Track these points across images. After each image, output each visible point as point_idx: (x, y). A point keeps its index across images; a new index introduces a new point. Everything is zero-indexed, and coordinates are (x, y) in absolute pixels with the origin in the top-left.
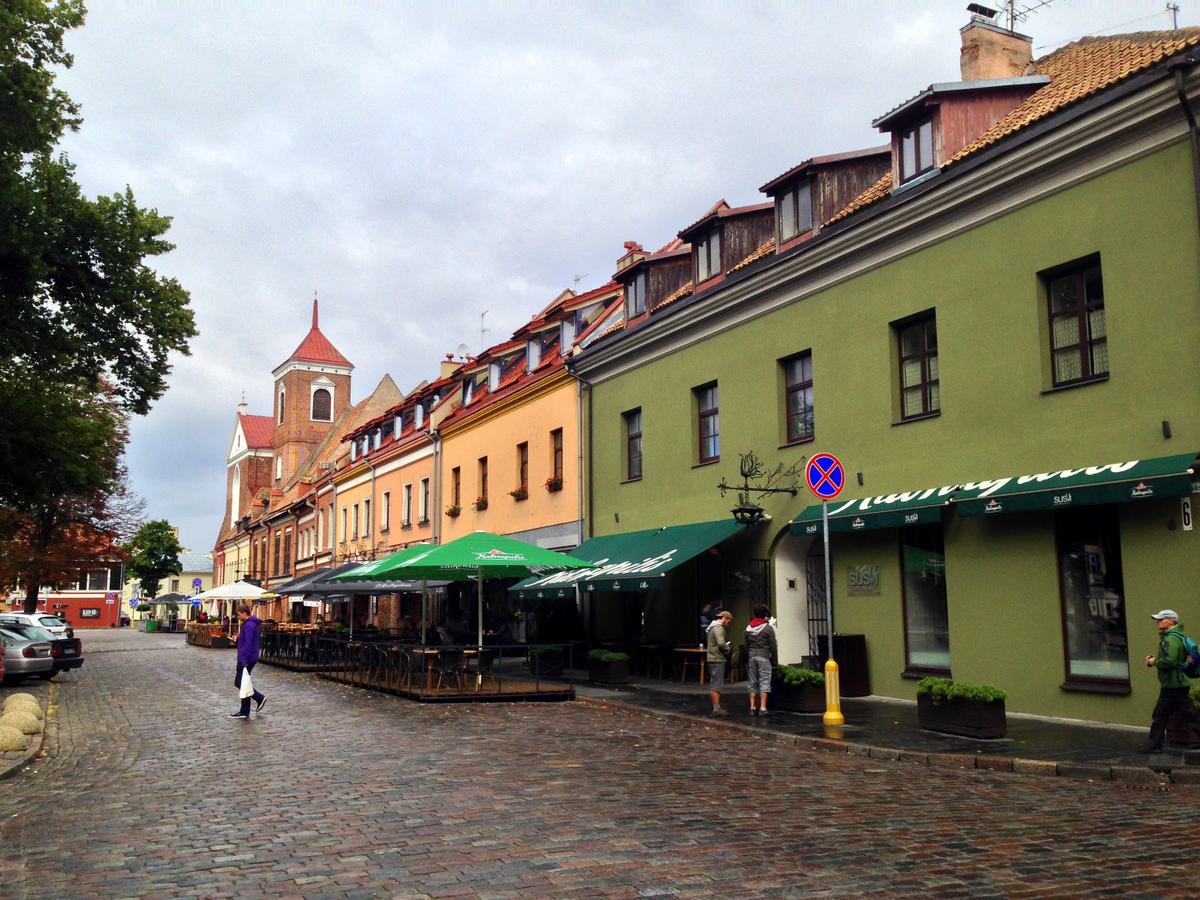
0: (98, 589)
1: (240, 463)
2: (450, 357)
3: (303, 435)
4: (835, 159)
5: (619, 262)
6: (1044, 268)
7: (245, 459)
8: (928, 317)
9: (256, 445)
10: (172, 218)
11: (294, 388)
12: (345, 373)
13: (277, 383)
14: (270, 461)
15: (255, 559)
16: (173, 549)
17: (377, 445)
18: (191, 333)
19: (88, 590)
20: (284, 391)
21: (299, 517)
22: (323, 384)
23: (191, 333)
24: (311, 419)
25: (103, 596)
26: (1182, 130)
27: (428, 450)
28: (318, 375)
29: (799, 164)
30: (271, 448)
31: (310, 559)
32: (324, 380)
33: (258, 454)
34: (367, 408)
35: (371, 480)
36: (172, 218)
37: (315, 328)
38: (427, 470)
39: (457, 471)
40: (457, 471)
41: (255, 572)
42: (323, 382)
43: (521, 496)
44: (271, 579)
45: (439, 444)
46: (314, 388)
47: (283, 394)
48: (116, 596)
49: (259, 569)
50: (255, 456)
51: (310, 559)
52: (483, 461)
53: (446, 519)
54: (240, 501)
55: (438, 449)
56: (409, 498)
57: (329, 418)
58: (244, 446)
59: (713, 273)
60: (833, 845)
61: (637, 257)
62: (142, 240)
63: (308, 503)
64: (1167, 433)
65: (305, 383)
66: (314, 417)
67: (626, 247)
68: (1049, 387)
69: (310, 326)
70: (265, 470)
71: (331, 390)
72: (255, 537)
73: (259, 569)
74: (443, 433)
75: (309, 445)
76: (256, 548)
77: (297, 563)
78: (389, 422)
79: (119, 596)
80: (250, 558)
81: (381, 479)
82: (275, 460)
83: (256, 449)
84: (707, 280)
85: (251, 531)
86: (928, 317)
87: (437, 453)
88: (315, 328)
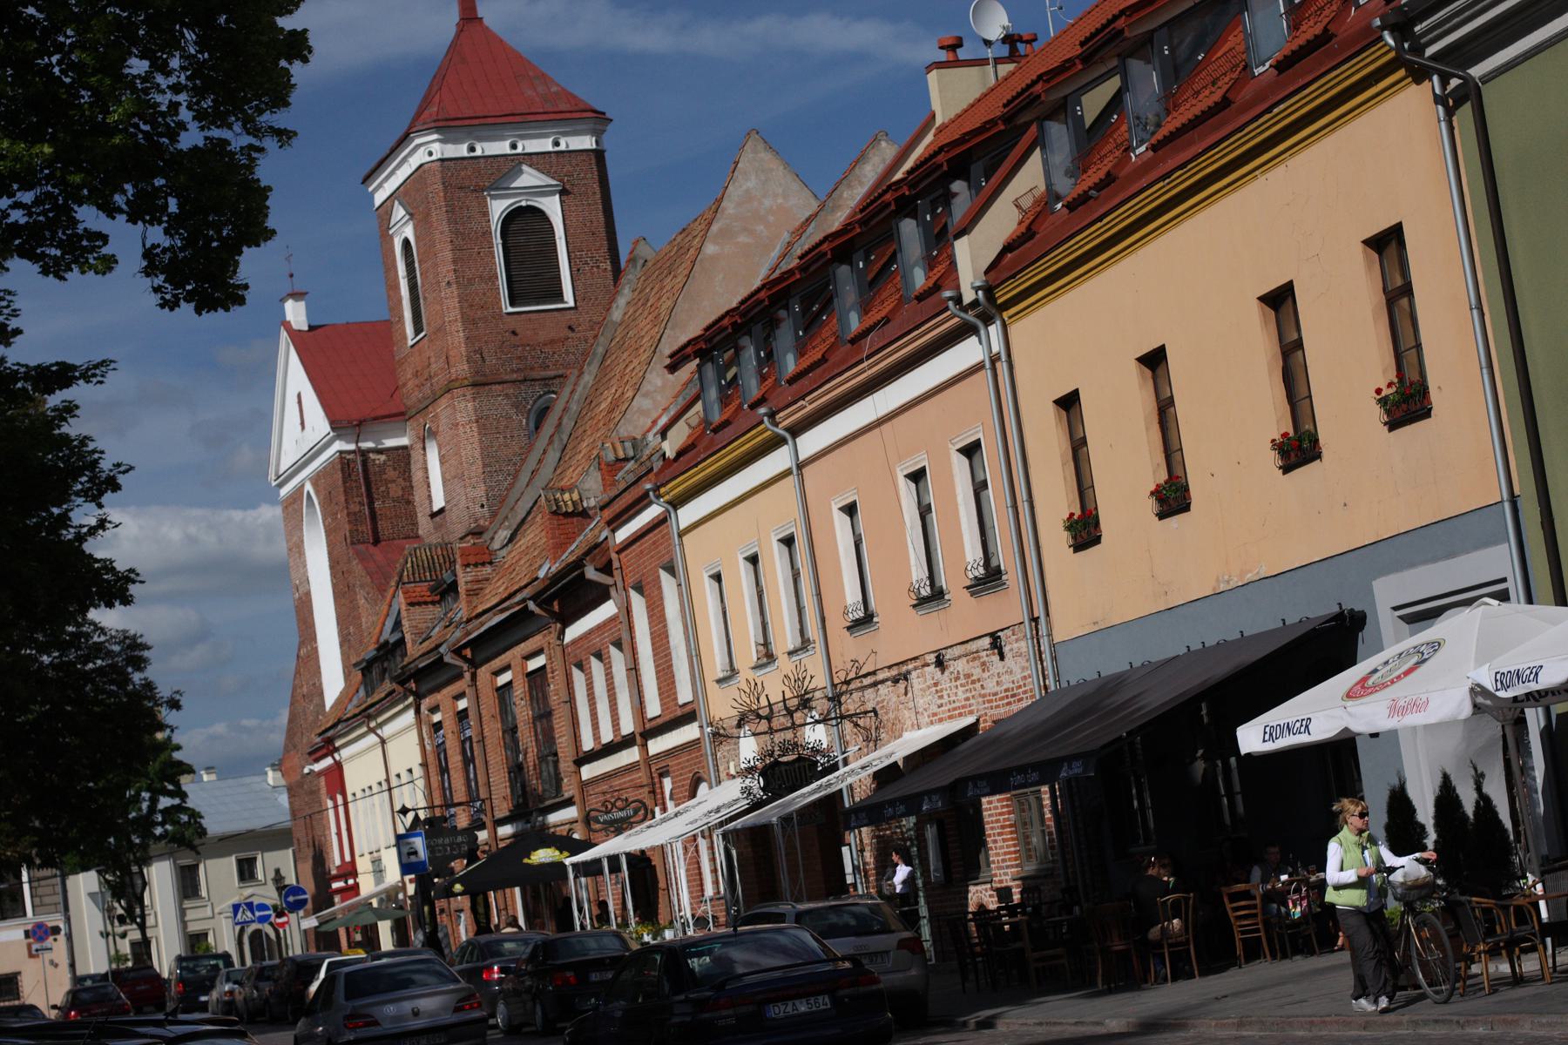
1: (316, 480)
3: (491, 361)
20: (409, 232)
27: (968, 353)
36: (19, 973)
46: (498, 208)
47: (406, 242)
55: (997, 346)
57: (559, 296)
70: (395, 491)
71: (552, 207)
73: (460, 794)
80: (424, 765)
82: (416, 455)
87: (994, 360)
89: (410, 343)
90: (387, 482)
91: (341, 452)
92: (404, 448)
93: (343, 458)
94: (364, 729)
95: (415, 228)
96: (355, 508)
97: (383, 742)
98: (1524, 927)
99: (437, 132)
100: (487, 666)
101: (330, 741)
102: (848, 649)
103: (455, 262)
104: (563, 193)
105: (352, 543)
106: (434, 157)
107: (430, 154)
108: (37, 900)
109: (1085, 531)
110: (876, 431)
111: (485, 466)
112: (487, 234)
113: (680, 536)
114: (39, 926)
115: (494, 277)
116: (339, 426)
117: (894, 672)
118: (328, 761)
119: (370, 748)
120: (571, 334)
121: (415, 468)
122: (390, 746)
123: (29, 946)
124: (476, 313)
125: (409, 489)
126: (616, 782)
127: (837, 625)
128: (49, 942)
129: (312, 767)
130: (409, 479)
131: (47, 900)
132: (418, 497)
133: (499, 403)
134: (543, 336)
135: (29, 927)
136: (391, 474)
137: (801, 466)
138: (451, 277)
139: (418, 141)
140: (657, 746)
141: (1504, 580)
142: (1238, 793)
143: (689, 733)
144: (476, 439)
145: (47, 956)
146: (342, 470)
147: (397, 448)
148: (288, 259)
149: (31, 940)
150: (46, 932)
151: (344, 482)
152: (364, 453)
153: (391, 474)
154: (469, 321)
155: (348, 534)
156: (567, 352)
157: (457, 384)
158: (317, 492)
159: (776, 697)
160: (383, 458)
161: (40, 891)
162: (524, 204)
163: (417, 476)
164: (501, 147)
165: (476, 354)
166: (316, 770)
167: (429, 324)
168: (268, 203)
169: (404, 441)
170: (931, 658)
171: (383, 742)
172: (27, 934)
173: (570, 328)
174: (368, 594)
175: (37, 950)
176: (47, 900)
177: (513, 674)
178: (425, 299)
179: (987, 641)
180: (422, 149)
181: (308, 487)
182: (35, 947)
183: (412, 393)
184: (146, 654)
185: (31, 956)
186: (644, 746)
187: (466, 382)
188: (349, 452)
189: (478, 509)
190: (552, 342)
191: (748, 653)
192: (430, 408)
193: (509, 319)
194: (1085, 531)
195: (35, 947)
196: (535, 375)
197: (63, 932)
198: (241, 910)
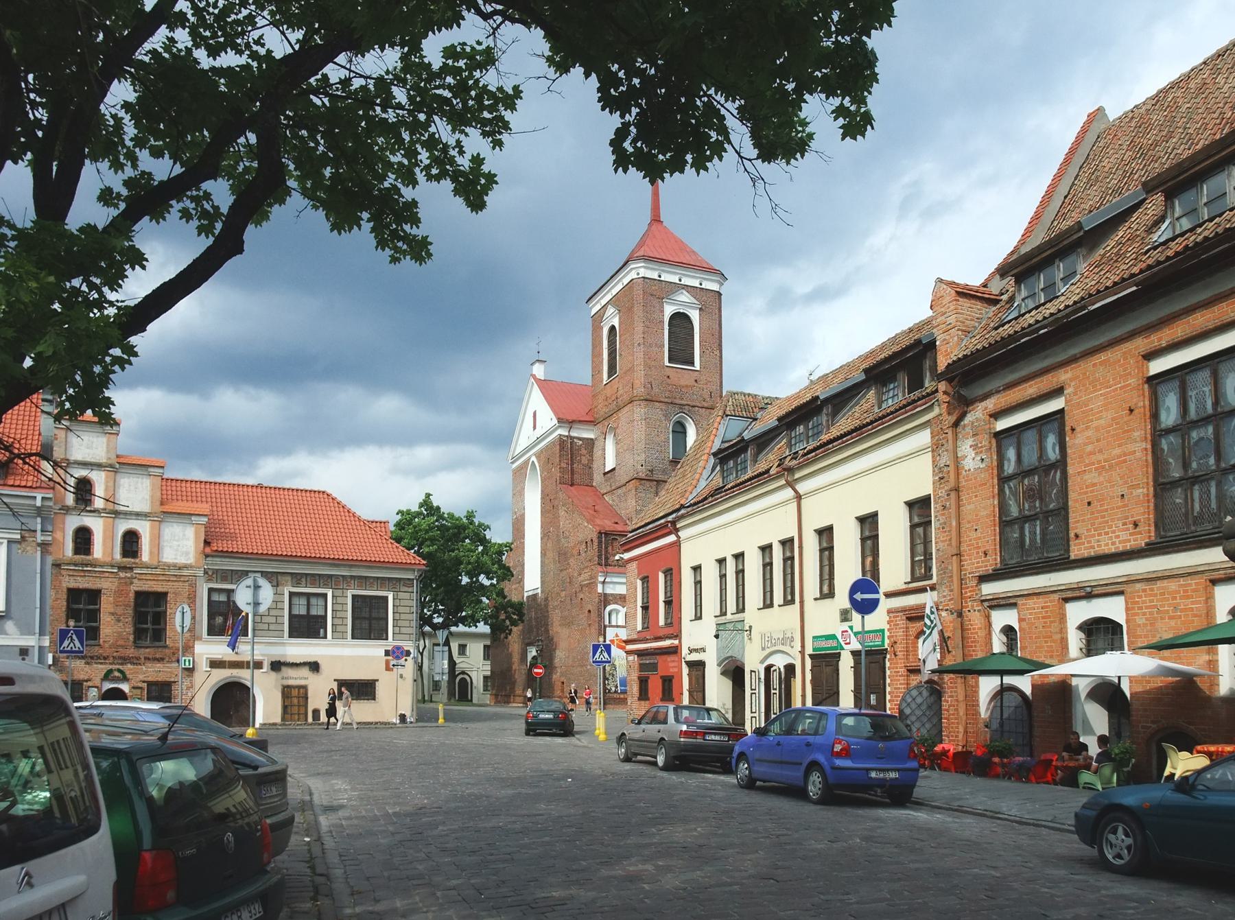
1: (538, 455)
3: (656, 390)
7: (552, 443)
8: (874, 515)
9: (570, 419)
10: (378, 680)
11: (638, 311)
12: (715, 287)
14: (590, 443)
18: (420, 223)
20: (616, 322)
22: (683, 303)
23: (420, 223)
24: (667, 364)
30: (593, 423)
33: (574, 434)
36: (378, 680)
37: (656, 219)
39: (697, 569)
42: (683, 302)
46: (669, 310)
47: (613, 328)
50: (569, 437)
54: (544, 512)
57: (692, 364)
58: (547, 420)
60: (1010, 810)
65: (655, 302)
68: (818, 596)
69: (647, 217)
70: (584, 460)
71: (695, 316)
82: (598, 444)
83: (571, 423)
86: (874, 515)
88: (656, 219)
89: (605, 383)
90: (581, 455)
91: (560, 435)
92: (592, 439)
93: (562, 441)
94: (783, 482)
95: (620, 318)
96: (564, 465)
97: (799, 497)
99: (644, 262)
100: (983, 404)
103: (644, 333)
104: (700, 309)
105: (560, 483)
106: (640, 276)
107: (638, 274)
108: (397, 629)
111: (646, 444)
114: (398, 648)
119: (785, 503)
120: (696, 385)
121: (597, 453)
122: (803, 501)
123: (387, 662)
124: (651, 363)
128: (402, 661)
129: (621, 556)
130: (592, 456)
131: (404, 630)
133: (657, 412)
134: (683, 382)
135: (390, 648)
136: (584, 451)
138: (641, 341)
139: (632, 266)
144: (644, 428)
145: (401, 670)
146: (560, 444)
147: (588, 439)
148: (538, 344)
149: (390, 658)
150: (402, 653)
151: (560, 451)
152: (572, 438)
153: (584, 451)
154: (648, 367)
155: (558, 478)
156: (693, 394)
157: (637, 398)
158: (539, 462)
160: (581, 442)
161: (400, 623)
162: (681, 311)
164: (674, 279)
166: (625, 558)
167: (620, 369)
168: (614, 157)
169: (592, 436)
171: (799, 497)
172: (387, 653)
173: (696, 381)
174: (568, 508)
175: (394, 665)
176: (404, 630)
177: (1067, 402)
178: (621, 355)
180: (634, 271)
181: (534, 459)
182: (392, 663)
185: (388, 669)
187: (642, 398)
188: (565, 436)
189: (640, 467)
190: (687, 386)
192: (614, 415)
193: (667, 369)
195: (392, 663)
196: (677, 401)
197: (412, 656)
198: (600, 650)
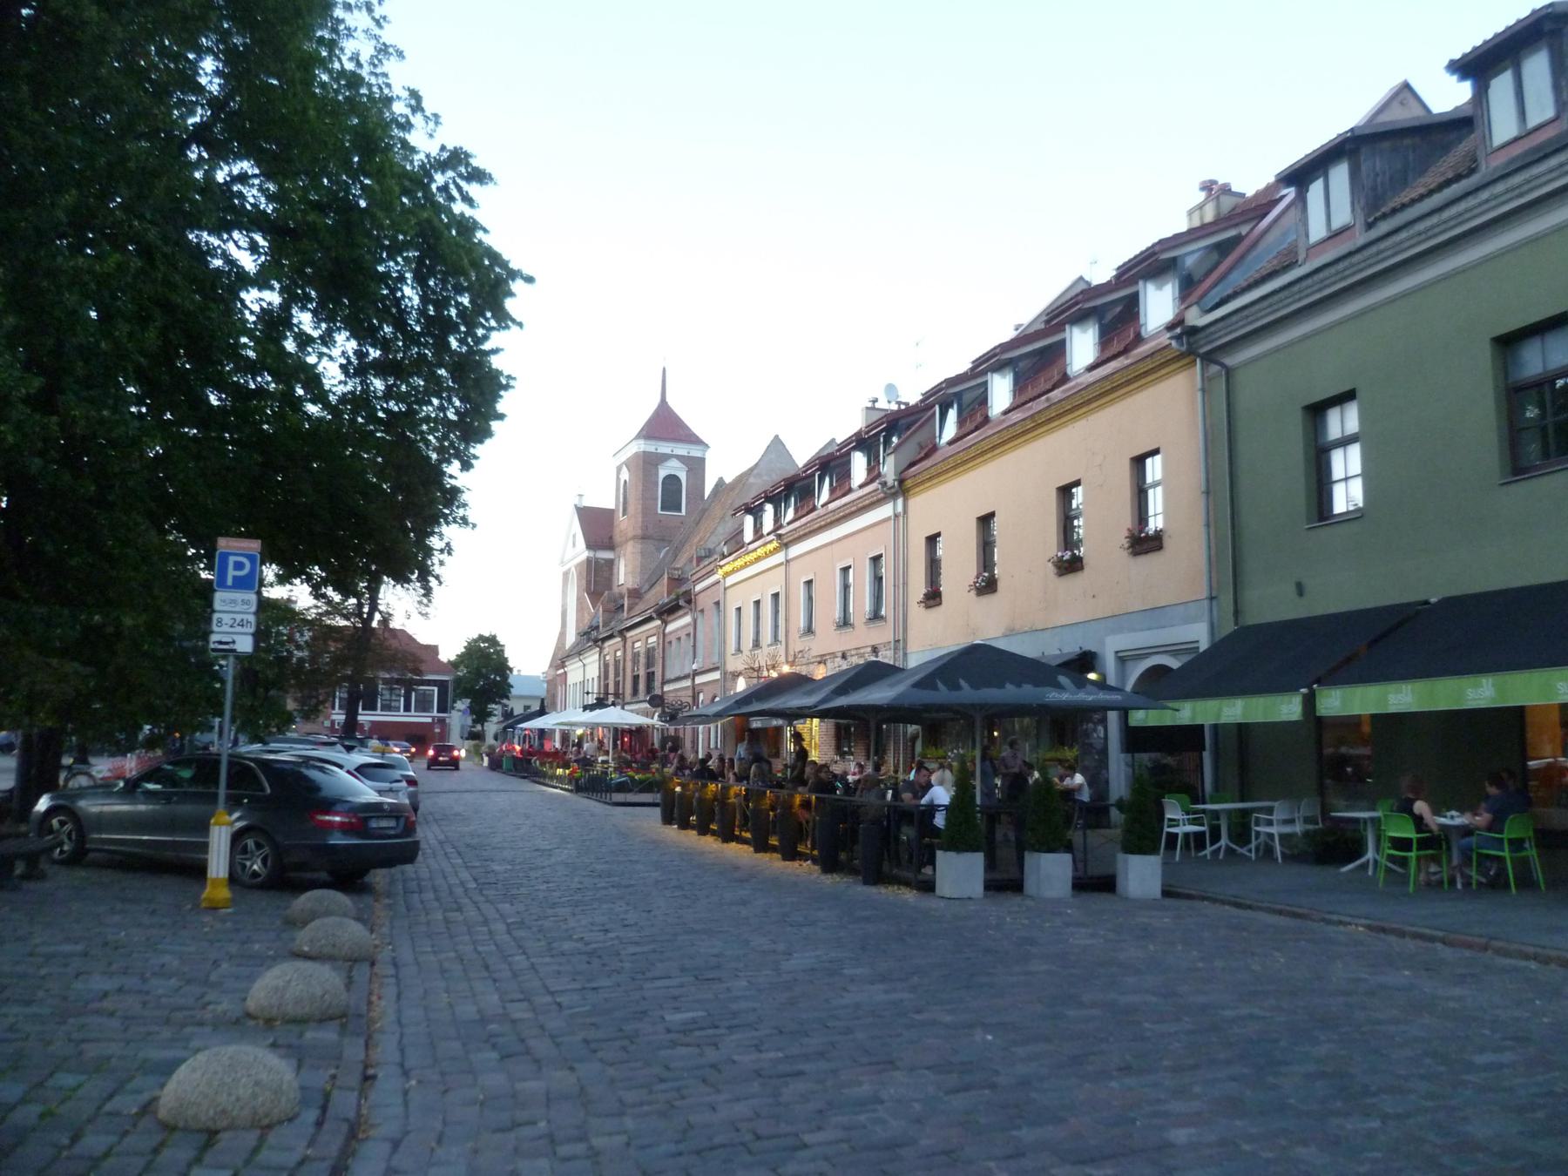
0: (424, 711)
2: (875, 401)
4: (1399, 126)
5: (1190, 213)
6: (1331, 395)
13: (619, 469)
15: (606, 677)
16: (502, 667)
17: (790, 514)
19: (413, 713)
21: (665, 623)
24: (659, 512)
25: (430, 720)
26: (88, 846)
27: (886, 511)
28: (666, 457)
29: (1335, 136)
31: (686, 677)
32: (674, 463)
34: (752, 480)
35: (781, 564)
38: (881, 544)
40: (739, 609)
41: (607, 694)
43: (845, 623)
44: (628, 703)
45: (900, 501)
46: (662, 473)
47: (625, 481)
48: (442, 721)
49: (611, 690)
51: (686, 677)
52: (986, 521)
53: (916, 612)
55: (900, 508)
56: (810, 598)
57: (680, 510)
59: (1533, 122)
61: (1227, 203)
62: (373, 568)
63: (681, 603)
64: (1300, 589)
66: (662, 509)
67: (1203, 189)
71: (683, 476)
72: (606, 651)
73: (611, 690)
74: (909, 483)
75: (656, 543)
76: (606, 666)
77: (664, 683)
78: (980, 380)
79: (448, 721)
80: (599, 677)
81: (798, 561)
82: (616, 562)
84: (1516, 140)
85: (600, 643)
87: (896, 516)
98: (804, 812)
101: (563, 662)
102: (797, 644)
109: (933, 597)
110: (829, 548)
112: (657, 482)
113: (725, 589)
115: (657, 499)
116: (589, 546)
117: (819, 659)
118: (561, 671)
121: (615, 568)
122: (587, 668)
124: (647, 511)
125: (612, 574)
126: (679, 694)
127: (794, 635)
132: (615, 577)
137: (788, 561)
140: (699, 680)
141: (1197, 642)
142: (1309, 702)
143: (716, 675)
159: (763, 664)
163: (615, 571)
165: (645, 527)
170: (840, 654)
179: (869, 649)
181: (573, 569)
183: (617, 538)
184: (473, 461)
186: (693, 679)
191: (747, 643)
194: (933, 597)
